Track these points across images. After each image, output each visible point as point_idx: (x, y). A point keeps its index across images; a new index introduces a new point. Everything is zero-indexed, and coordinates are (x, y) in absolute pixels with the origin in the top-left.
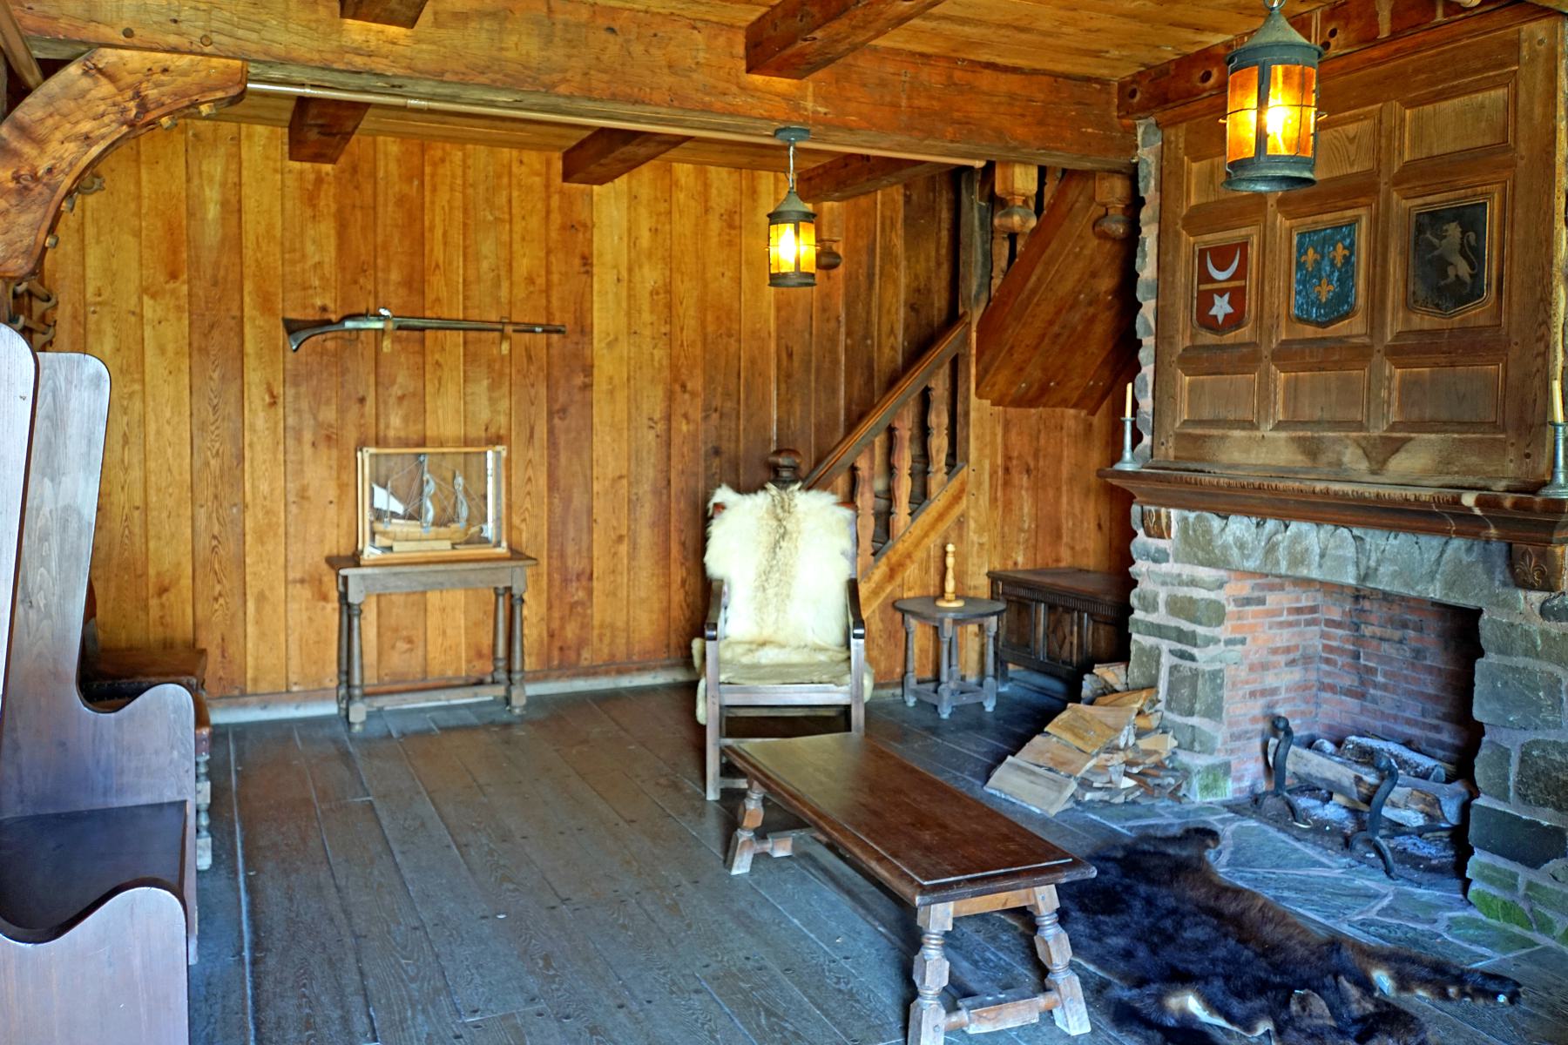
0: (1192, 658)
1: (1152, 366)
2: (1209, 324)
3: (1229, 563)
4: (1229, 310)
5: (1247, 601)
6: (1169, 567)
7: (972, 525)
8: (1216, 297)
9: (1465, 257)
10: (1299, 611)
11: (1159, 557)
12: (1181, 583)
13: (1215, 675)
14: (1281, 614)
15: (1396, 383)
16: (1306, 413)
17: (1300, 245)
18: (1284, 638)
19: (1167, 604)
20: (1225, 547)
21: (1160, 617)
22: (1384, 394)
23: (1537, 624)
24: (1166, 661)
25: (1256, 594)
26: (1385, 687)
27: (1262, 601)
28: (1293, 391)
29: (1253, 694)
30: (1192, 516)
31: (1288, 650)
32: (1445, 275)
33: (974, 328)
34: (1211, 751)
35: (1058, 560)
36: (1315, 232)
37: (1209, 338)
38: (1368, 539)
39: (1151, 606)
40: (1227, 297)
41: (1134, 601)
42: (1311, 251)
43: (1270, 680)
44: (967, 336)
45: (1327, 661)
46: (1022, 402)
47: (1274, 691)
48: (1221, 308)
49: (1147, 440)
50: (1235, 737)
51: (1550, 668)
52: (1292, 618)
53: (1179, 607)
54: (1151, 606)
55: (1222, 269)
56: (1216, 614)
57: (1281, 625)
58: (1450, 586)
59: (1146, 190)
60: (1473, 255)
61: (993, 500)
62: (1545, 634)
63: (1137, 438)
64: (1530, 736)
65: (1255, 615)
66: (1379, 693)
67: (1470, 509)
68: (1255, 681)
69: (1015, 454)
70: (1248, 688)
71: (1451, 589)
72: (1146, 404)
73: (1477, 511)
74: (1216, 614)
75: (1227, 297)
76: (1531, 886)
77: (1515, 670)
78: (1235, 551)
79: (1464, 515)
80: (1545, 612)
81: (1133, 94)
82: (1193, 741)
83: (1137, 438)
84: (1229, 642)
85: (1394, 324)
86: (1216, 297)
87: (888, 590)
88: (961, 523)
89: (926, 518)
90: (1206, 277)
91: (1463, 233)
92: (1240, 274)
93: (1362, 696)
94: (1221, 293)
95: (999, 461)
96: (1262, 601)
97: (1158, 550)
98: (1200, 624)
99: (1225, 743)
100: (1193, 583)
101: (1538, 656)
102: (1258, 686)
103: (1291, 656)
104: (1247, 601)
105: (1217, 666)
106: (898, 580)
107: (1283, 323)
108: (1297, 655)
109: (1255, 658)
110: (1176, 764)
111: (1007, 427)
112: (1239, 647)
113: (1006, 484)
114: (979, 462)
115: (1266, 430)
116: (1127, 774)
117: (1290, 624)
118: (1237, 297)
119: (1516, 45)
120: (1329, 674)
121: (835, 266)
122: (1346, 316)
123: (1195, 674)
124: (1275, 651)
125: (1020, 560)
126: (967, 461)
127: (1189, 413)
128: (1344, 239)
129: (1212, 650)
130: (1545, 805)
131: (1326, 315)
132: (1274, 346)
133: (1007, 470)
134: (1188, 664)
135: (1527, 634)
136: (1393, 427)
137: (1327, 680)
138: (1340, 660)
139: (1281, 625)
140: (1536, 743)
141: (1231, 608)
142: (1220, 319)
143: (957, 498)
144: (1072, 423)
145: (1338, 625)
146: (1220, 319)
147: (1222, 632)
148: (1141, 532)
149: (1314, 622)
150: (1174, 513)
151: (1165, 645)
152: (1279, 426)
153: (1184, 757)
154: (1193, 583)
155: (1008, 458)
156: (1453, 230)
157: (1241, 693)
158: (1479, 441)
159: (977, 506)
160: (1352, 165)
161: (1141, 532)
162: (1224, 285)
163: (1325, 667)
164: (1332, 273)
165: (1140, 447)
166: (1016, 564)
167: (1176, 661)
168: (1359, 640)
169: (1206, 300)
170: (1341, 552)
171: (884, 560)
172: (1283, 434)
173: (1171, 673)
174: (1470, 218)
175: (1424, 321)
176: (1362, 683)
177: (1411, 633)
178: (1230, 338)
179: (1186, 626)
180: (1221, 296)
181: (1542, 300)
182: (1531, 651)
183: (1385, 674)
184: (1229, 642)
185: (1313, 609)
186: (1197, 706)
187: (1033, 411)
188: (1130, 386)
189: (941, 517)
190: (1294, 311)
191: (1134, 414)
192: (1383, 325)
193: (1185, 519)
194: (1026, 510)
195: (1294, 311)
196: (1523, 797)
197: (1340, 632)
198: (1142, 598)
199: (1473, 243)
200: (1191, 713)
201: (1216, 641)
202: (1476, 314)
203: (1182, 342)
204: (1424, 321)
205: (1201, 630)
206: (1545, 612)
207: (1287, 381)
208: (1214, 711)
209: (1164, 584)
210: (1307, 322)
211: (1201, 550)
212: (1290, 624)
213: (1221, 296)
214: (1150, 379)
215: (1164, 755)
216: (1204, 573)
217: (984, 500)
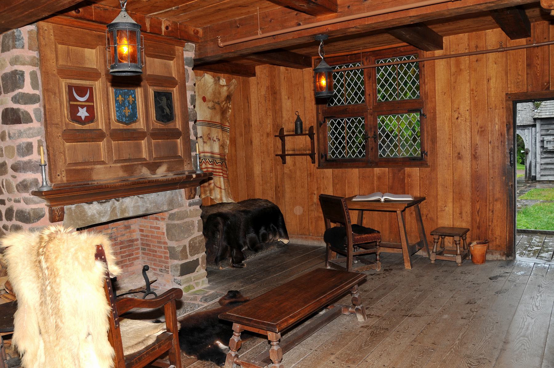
4: (87, 115)
32: (164, 112)
40: (85, 109)
48: (83, 113)
51: (191, 219)
62: (190, 210)
75: (85, 109)
78: (97, 215)
86: (80, 109)
94: (82, 107)
131: (128, 120)
142: (83, 118)
156: (164, 99)
162: (84, 104)
172: (119, 165)
174: (169, 96)
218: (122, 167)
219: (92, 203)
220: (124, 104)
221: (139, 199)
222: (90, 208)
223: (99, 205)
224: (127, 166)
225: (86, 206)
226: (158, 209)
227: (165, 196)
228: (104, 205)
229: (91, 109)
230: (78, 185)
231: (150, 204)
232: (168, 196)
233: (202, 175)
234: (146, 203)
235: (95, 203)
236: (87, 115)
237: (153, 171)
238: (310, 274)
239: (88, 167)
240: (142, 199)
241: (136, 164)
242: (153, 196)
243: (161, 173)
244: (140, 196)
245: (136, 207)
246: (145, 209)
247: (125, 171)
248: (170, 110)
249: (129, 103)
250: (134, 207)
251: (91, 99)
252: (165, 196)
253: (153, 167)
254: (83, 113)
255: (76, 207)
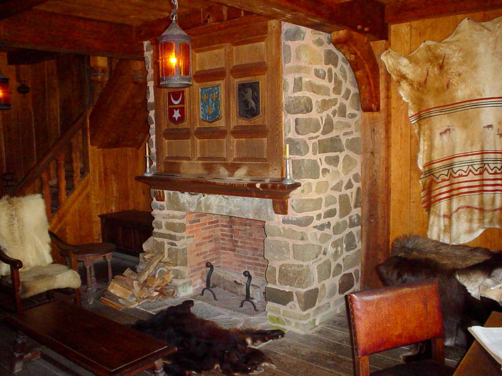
0: (175, 245)
1: (154, 136)
2: (172, 119)
3: (185, 210)
4: (180, 116)
5: (194, 222)
6: (166, 212)
7: (93, 197)
8: (175, 111)
9: (254, 100)
10: (212, 223)
11: (162, 208)
12: (170, 218)
13: (184, 250)
14: (206, 225)
15: (235, 144)
16: (207, 154)
17: (202, 93)
18: (207, 233)
19: (166, 226)
20: (184, 204)
21: (164, 231)
22: (231, 148)
23: (282, 225)
24: (167, 247)
25: (197, 218)
26: (241, 247)
27: (199, 221)
28: (203, 146)
29: (198, 255)
30: (172, 192)
31: (209, 237)
32: (248, 107)
33: (88, 118)
34: (183, 278)
35: (128, 207)
36: (206, 88)
37: (173, 126)
38: (230, 199)
39: (160, 227)
40: (178, 111)
41: (154, 225)
42: (205, 95)
43: (204, 249)
44: (85, 120)
45: (223, 239)
46: (110, 145)
47: (205, 252)
48: (177, 115)
49: (155, 164)
50: (192, 271)
51: (286, 239)
52: (210, 226)
53: (170, 226)
54: (160, 227)
55: (176, 100)
56: (182, 228)
57: (206, 228)
58: (256, 214)
59: (148, 69)
60: (256, 99)
61: (101, 186)
62: (284, 228)
63: (151, 163)
64: (281, 263)
65: (197, 226)
66: (240, 249)
67: (259, 189)
68: (198, 250)
69: (109, 167)
70: (196, 253)
71: (256, 215)
72: (154, 150)
73: (261, 189)
74: (182, 228)
75: (178, 111)
76: (284, 311)
77: (276, 241)
78: (187, 205)
79: (257, 190)
80: (284, 222)
81: (141, 31)
82: (178, 275)
83: (151, 163)
84: (188, 237)
85: (233, 124)
86: (175, 111)
87: (59, 226)
88: (88, 197)
89: (73, 196)
90: (171, 103)
91: (253, 92)
92: (182, 102)
93: (234, 250)
94: (176, 109)
95: (102, 170)
96: (199, 221)
97: (161, 206)
98: (177, 232)
99: (189, 274)
100: (173, 217)
101: (283, 236)
102: (199, 252)
103: (210, 239)
104: (194, 222)
105: (185, 247)
106: (63, 222)
107: (198, 121)
108: (212, 239)
109: (197, 242)
110: (172, 284)
111: (104, 155)
112: (192, 239)
113: (106, 180)
114: (94, 171)
115: (194, 161)
116: (156, 291)
117: (209, 228)
118: (182, 111)
119: (266, 28)
120: (223, 244)
121: (28, 92)
122: (218, 119)
123: (177, 251)
124: (205, 238)
125: (114, 208)
126: (89, 171)
127: (169, 153)
128: (216, 91)
129: (182, 241)
130: (287, 285)
131: (211, 119)
132: (195, 129)
133: (106, 174)
134: (174, 247)
135: (279, 230)
136: (235, 160)
137: (223, 246)
138: (226, 238)
139: (206, 228)
140: (283, 265)
141: (188, 225)
142: (177, 119)
143: (85, 187)
144: (130, 154)
145: (225, 226)
146: (177, 119)
147: (185, 234)
148: (154, 199)
149: (218, 226)
150: (165, 191)
151: (166, 241)
152: (199, 159)
153: (175, 282)
154: (173, 217)
155: (106, 169)
156: (250, 91)
157: (193, 255)
158: (261, 164)
159: (94, 189)
160: (217, 64)
161: (154, 199)
163: (222, 241)
164: (213, 103)
165: (152, 166)
166: (112, 210)
167: (170, 246)
168: (232, 231)
169: (171, 112)
170: (221, 204)
171: (56, 215)
172: (200, 162)
173: (168, 251)
174: (254, 87)
175: (243, 122)
176: (234, 246)
177: (248, 227)
178: (181, 126)
179: (172, 233)
180: (176, 110)
181: (277, 116)
182: (280, 235)
183: (241, 242)
184: (188, 237)
185: (217, 222)
186: (178, 262)
187: (115, 149)
188: (147, 144)
189: (80, 194)
190: (201, 117)
191: (149, 154)
192: (230, 124)
193: (169, 194)
194: (114, 189)
195: (201, 117)
196: (280, 283)
197: (226, 229)
198: (156, 224)
199: (256, 96)
200: (177, 265)
201: (183, 238)
202: (258, 120)
203: (164, 127)
204: (243, 122)
205: (178, 234)
206: (284, 222)
207: (200, 143)
208: (185, 263)
209: (164, 218)
210: (206, 121)
211: (176, 205)
212: (209, 228)
213: (176, 110)
214: (154, 140)
215: (169, 281)
216: (177, 213)
217: (97, 187)
218: (203, 164)
219: (184, 193)
220: (208, 102)
221: (224, 199)
222: (182, 197)
223: (189, 196)
224: (207, 164)
225: (179, 194)
226: (242, 214)
227: (252, 203)
228: (194, 197)
229: (182, 111)
230: (388, 169)
231: (234, 207)
232: (255, 203)
233: (270, 186)
234: (230, 205)
235: (186, 193)
236: (180, 116)
237: (232, 174)
238: (273, 289)
239: (177, 161)
240: (226, 200)
241: (215, 163)
242: (238, 200)
243: (241, 176)
244: (226, 196)
245: (220, 207)
246: (228, 211)
247: (206, 169)
248: (256, 104)
249: (212, 101)
250: (218, 206)
251: (182, 102)
252: (252, 203)
253: (233, 168)
254: (177, 115)
255: (173, 193)
